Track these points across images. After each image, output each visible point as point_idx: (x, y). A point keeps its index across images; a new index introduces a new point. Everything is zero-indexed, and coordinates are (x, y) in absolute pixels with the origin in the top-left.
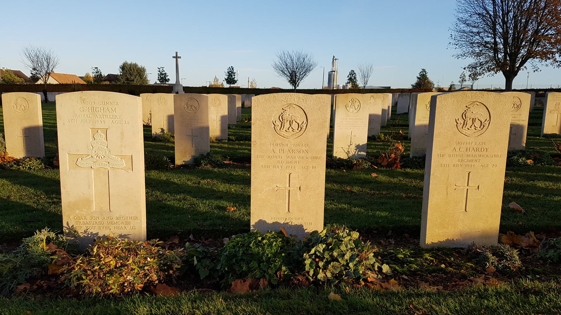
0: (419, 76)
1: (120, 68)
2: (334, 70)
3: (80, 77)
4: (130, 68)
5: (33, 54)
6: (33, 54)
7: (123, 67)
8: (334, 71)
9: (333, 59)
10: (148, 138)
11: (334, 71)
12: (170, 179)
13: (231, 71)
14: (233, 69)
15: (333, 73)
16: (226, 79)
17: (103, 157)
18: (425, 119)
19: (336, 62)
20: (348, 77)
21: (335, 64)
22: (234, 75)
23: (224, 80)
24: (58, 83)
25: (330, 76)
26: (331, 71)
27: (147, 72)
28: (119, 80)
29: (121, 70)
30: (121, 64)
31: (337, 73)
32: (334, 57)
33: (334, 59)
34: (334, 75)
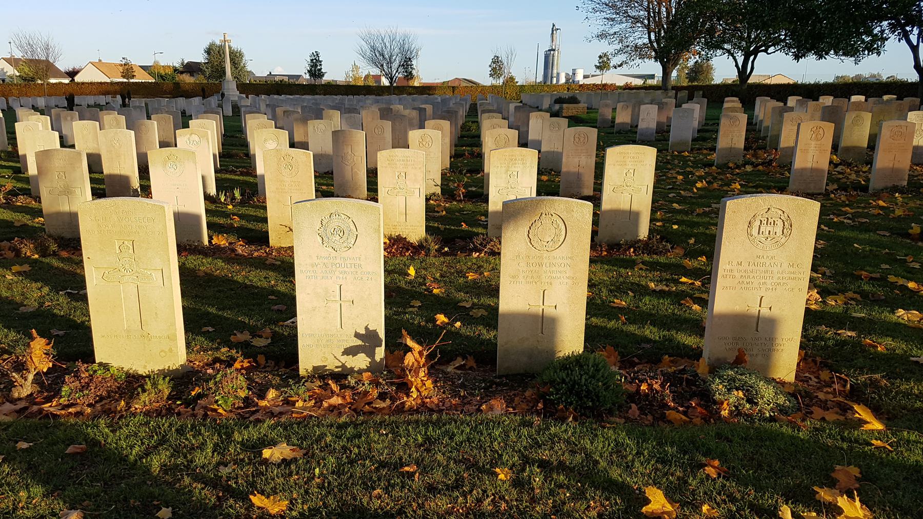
0: (598, 65)
1: (205, 52)
2: (554, 48)
3: (140, 66)
4: (219, 52)
5: (24, 41)
6: (24, 41)
7: (208, 51)
8: (554, 50)
9: (553, 28)
10: (614, 246)
11: (554, 50)
12: (208, 359)
13: (315, 59)
14: (317, 55)
15: (552, 52)
16: (309, 71)
17: (131, 271)
18: (633, 160)
19: (557, 34)
20: (490, 66)
21: (554, 38)
22: (321, 65)
23: (306, 72)
24: (108, 81)
25: (547, 57)
26: (549, 50)
27: (246, 57)
28: (203, 72)
29: (206, 55)
30: (206, 45)
31: (558, 53)
32: (554, 25)
33: (554, 30)
34: (553, 56)
